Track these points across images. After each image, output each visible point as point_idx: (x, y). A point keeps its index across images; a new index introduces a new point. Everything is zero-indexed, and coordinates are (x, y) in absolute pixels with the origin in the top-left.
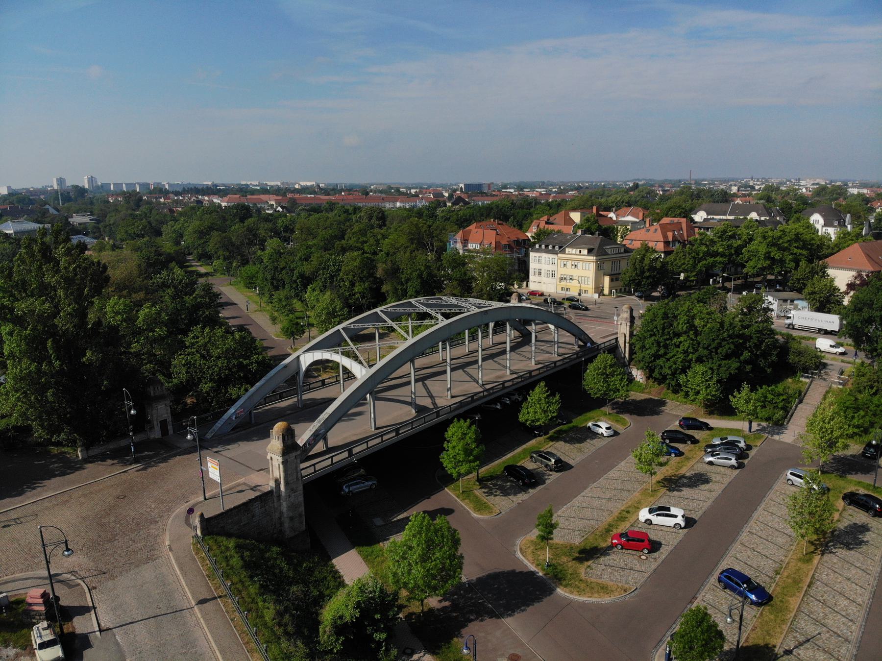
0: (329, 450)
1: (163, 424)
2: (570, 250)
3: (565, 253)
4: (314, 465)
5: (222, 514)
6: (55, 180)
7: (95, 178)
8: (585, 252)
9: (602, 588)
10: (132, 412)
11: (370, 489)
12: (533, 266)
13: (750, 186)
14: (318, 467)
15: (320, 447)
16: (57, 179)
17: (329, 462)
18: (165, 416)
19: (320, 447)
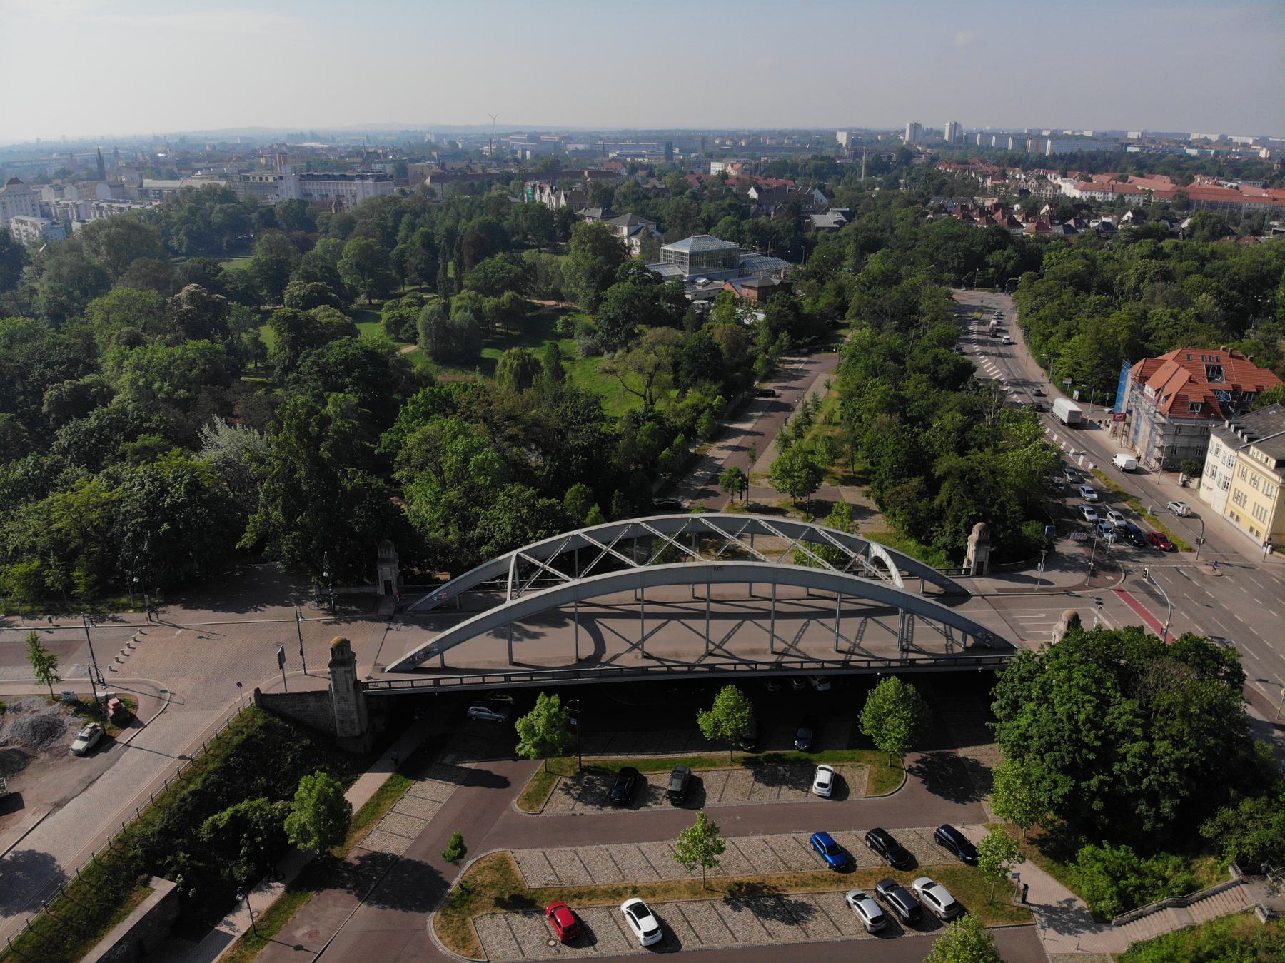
0: (445, 669)
1: (388, 585)
2: (1256, 450)
3: (1247, 453)
4: (412, 681)
5: (281, 695)
6: (908, 125)
7: (960, 126)
8: (1273, 463)
9: (826, 880)
10: (135, 580)
11: (495, 722)
12: (1211, 458)
13: (976, 412)
14: (416, 684)
15: (434, 662)
16: (911, 125)
17: (458, 681)
18: (389, 578)
19: (434, 662)
